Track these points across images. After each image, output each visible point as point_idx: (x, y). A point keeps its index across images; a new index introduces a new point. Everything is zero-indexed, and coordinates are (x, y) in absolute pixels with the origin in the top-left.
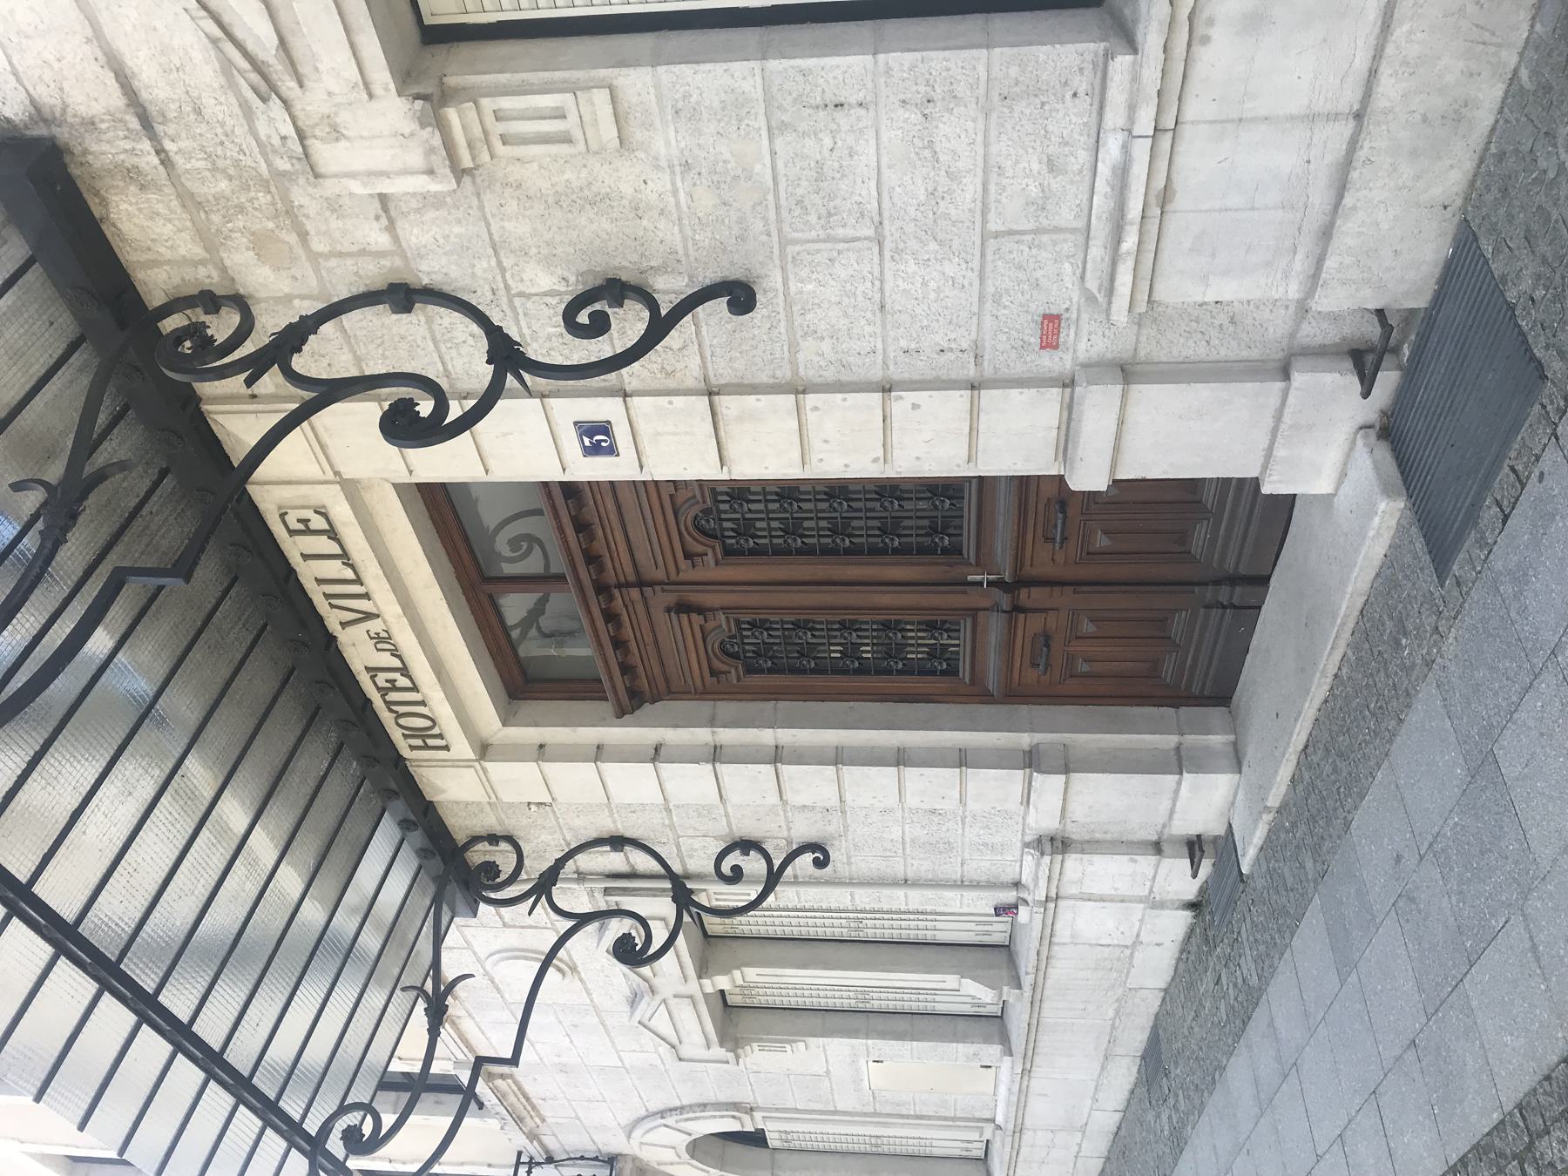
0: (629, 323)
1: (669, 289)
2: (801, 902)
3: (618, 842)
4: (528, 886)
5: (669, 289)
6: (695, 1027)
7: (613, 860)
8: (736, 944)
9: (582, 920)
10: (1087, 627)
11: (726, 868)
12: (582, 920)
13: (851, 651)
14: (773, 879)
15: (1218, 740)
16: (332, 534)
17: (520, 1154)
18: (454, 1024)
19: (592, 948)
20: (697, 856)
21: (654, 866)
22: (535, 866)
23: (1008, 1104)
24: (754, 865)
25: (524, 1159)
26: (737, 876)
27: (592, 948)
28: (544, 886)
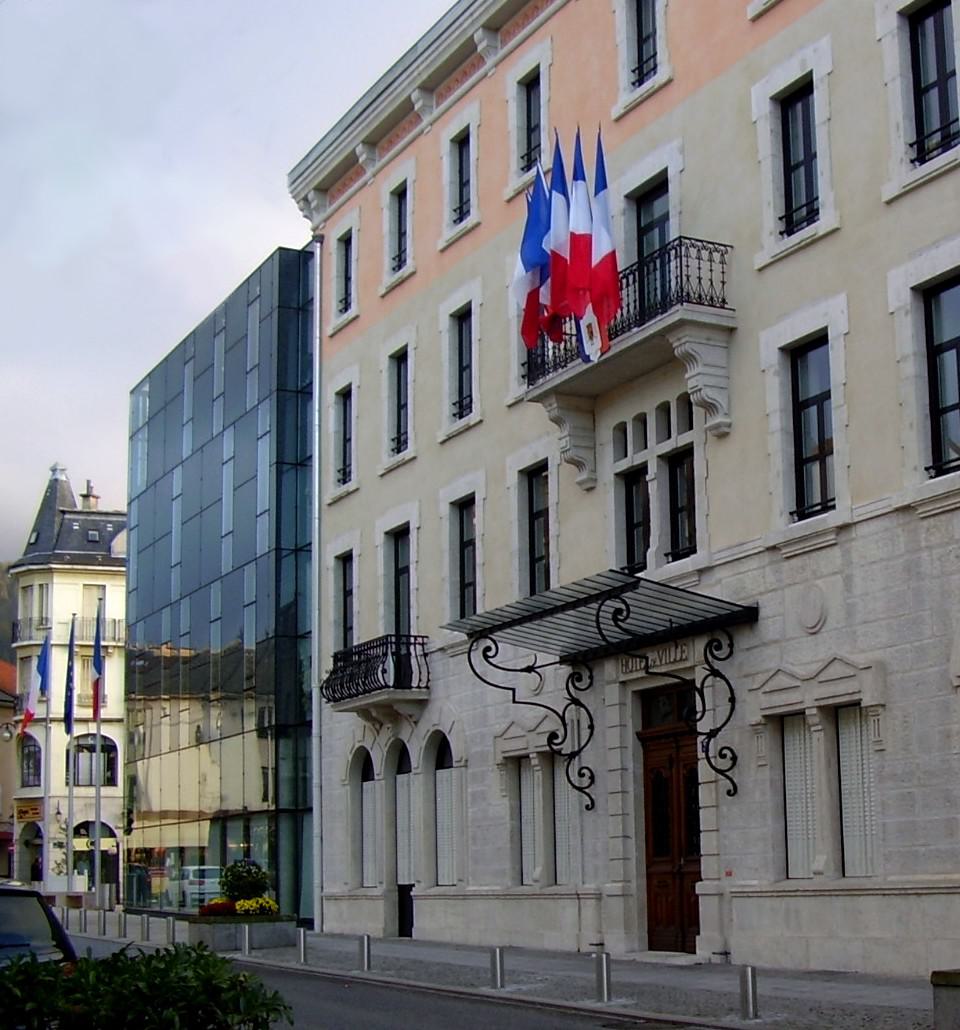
0: (724, 764)
1: (734, 774)
2: (568, 800)
3: (591, 727)
4: (573, 694)
5: (734, 774)
6: (515, 747)
7: (585, 723)
8: (516, 780)
9: (563, 718)
10: (670, 899)
11: (585, 771)
12: (563, 718)
13: (416, 639)
14: (580, 789)
15: (636, 946)
16: (681, 660)
17: (427, 637)
18: (580, 758)
19: (553, 724)
20: (588, 758)
21: (582, 744)
22: (583, 698)
23: (487, 891)
24: (586, 781)
25: (425, 640)
26: (581, 775)
27: (553, 724)
28: (575, 701)
